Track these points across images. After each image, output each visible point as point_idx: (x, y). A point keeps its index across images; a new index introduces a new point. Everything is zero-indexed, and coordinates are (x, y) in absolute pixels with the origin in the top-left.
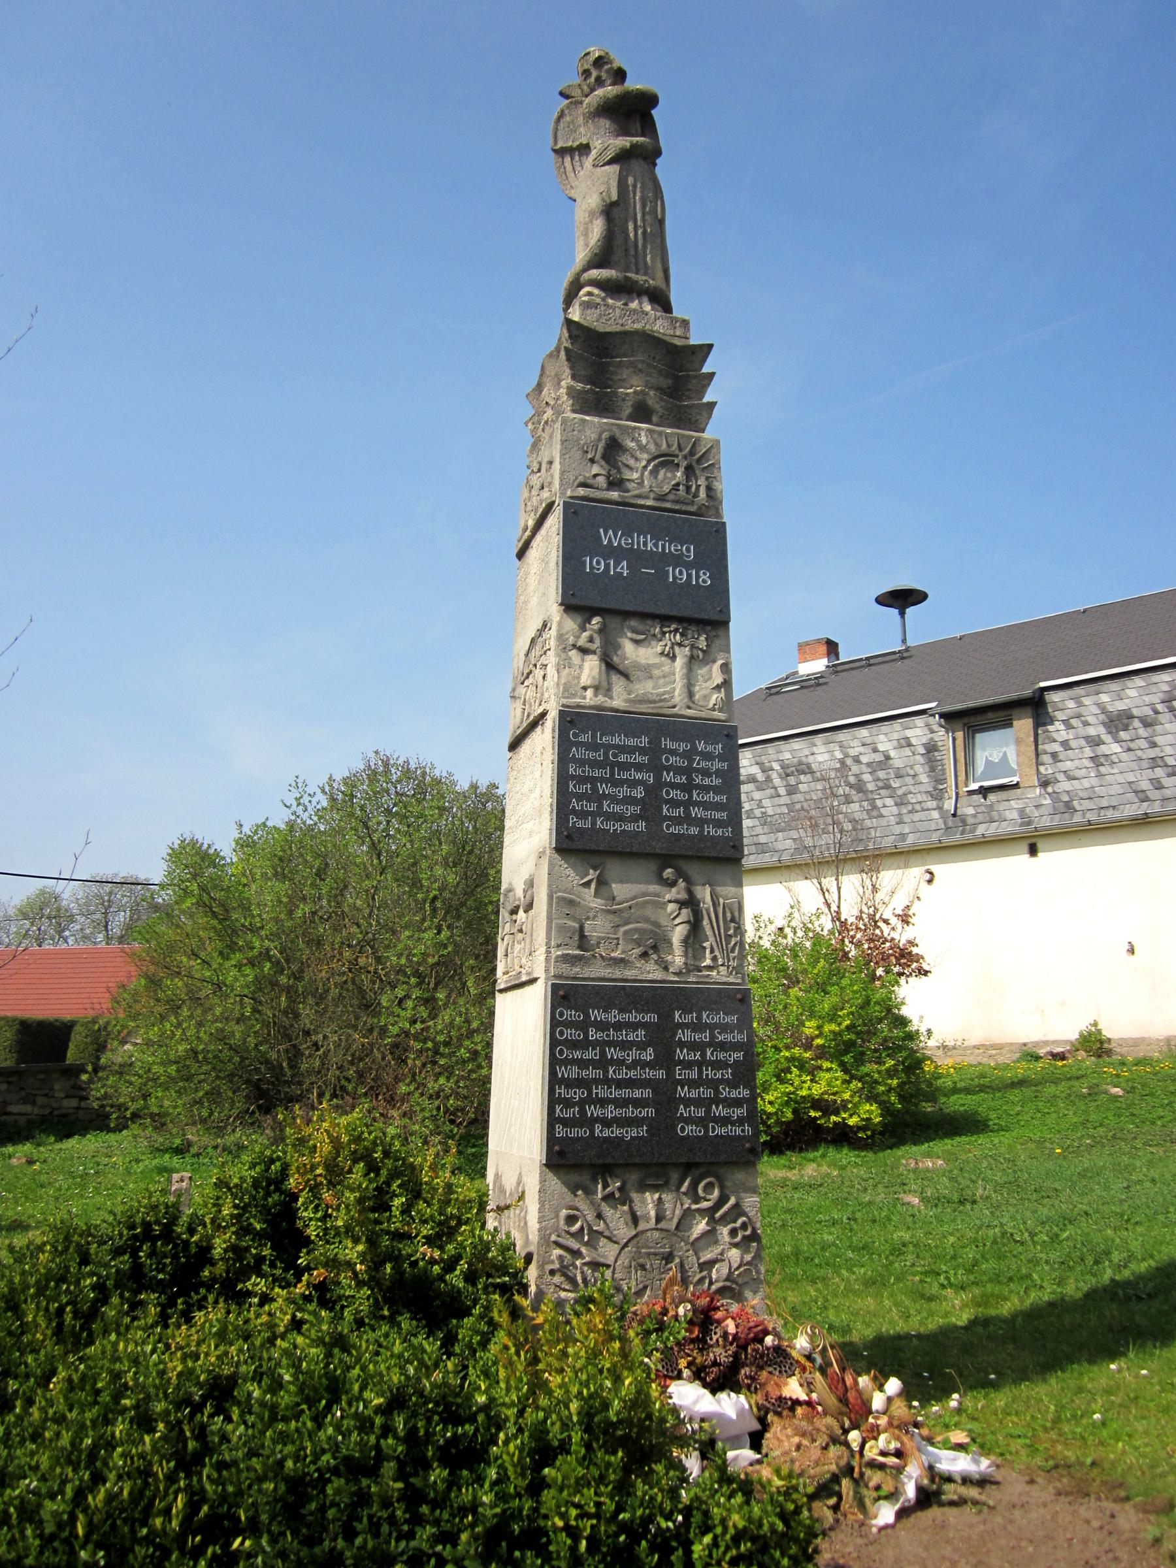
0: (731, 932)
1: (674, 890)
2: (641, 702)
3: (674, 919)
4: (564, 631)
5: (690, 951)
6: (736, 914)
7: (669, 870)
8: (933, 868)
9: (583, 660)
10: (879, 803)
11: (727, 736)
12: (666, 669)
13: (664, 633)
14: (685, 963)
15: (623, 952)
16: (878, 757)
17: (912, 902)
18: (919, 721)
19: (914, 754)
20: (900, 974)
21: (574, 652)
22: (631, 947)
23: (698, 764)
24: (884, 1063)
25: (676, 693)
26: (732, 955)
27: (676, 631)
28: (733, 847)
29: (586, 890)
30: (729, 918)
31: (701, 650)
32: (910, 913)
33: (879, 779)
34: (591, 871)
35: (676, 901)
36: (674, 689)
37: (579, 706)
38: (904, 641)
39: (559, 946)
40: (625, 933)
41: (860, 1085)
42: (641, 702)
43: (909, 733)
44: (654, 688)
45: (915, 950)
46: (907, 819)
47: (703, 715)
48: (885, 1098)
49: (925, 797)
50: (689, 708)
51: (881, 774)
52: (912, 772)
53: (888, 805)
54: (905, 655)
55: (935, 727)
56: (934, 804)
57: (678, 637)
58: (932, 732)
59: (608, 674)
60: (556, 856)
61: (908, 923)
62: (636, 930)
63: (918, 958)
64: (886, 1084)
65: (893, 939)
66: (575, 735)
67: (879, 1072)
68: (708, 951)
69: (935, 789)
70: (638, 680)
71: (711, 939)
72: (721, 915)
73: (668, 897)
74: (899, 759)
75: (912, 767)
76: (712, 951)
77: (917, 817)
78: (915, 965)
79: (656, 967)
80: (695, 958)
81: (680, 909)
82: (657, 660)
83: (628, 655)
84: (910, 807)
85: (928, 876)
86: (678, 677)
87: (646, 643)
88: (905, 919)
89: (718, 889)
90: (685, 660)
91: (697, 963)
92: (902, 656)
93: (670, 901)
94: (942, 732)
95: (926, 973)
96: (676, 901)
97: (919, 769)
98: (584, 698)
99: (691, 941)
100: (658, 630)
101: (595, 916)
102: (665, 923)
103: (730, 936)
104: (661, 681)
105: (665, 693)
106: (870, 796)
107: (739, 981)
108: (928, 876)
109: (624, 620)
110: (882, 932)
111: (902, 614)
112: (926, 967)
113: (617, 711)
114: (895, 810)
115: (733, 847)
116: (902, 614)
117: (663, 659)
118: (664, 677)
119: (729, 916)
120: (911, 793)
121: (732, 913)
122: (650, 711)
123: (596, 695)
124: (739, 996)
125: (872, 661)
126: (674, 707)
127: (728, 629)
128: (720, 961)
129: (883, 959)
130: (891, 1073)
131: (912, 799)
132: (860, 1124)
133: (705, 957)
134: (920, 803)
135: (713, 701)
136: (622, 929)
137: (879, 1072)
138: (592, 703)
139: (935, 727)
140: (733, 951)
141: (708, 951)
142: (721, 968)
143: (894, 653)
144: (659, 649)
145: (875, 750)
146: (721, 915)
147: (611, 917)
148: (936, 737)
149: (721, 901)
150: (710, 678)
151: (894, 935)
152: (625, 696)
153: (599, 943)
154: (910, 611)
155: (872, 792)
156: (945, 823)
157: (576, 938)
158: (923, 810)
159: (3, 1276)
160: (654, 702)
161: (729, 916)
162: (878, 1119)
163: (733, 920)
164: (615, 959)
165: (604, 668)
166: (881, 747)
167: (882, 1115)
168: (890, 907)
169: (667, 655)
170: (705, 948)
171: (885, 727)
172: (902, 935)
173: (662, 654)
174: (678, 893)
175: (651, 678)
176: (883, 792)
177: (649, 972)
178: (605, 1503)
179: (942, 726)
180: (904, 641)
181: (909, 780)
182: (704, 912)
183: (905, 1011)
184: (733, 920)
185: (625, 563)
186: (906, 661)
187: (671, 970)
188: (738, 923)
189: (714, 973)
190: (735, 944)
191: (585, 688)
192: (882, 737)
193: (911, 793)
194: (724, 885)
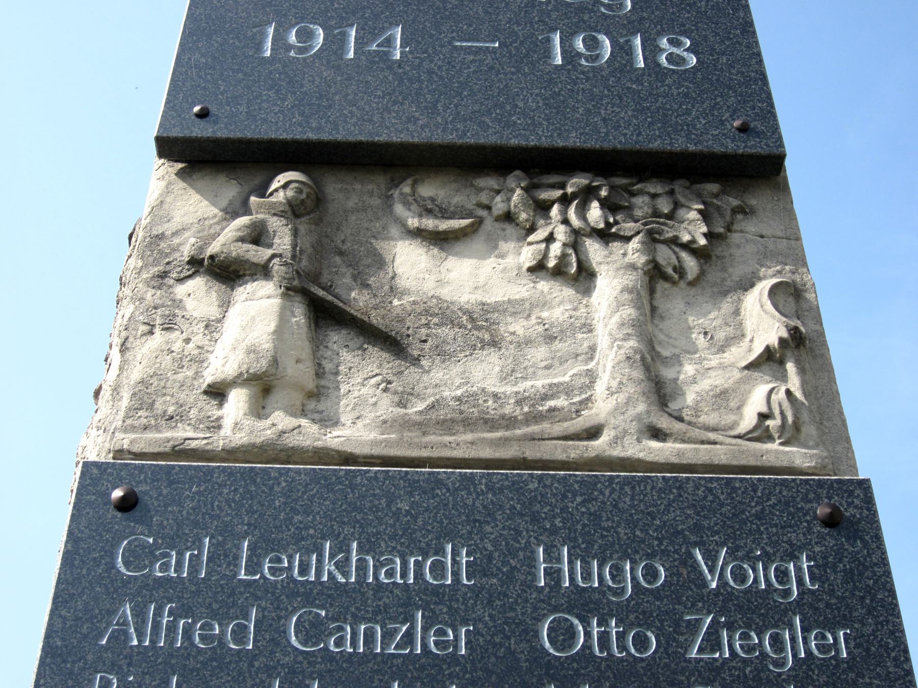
2: (447, 426)
4: (168, 228)
9: (225, 305)
11: (832, 521)
12: (557, 314)
13: (543, 208)
21: (198, 284)
23: (712, 642)
25: (600, 388)
27: (586, 195)
31: (689, 247)
36: (592, 376)
37: (179, 452)
42: (447, 426)
44: (504, 378)
47: (720, 454)
50: (657, 434)
57: (595, 213)
59: (317, 344)
66: (133, 559)
70: (443, 354)
82: (522, 290)
83: (402, 283)
86: (603, 336)
87: (478, 243)
90: (631, 279)
98: (216, 425)
100: (517, 196)
104: (539, 353)
105: (552, 392)
109: (395, 183)
113: (348, 459)
117: (544, 285)
118: (550, 338)
122: (487, 453)
123: (259, 409)
126: (593, 433)
127: (783, 188)
135: (755, 403)
138: (240, 439)
144: (527, 255)
150: (738, 336)
152: (386, 408)
160: (510, 422)
165: (299, 316)
169: (559, 272)
173: (538, 268)
175: (495, 343)
178: (715, 130)
185: (398, 32)
191: (218, 392)
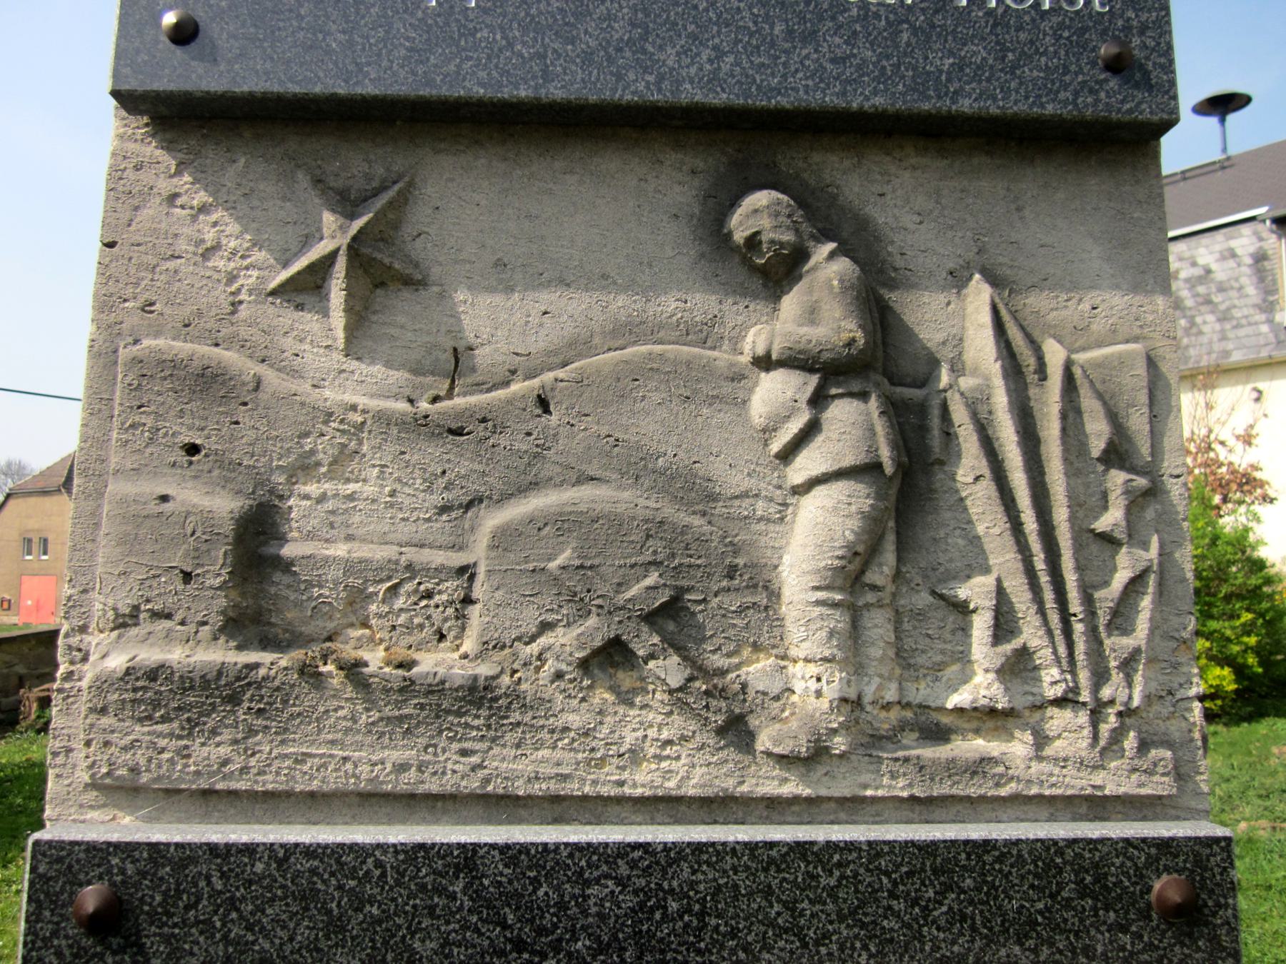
0: (1112, 519)
1: (791, 303)
3: (787, 454)
5: (878, 626)
6: (1138, 422)
7: (761, 198)
8: (1260, 385)
10: (1198, 320)
14: (850, 703)
15: (490, 647)
16: (1197, 272)
17: (1256, 421)
18: (1246, 229)
19: (1239, 265)
20: (1240, 502)
22: (530, 618)
24: (1239, 617)
26: (1118, 646)
28: (1116, 66)
29: (309, 321)
30: (1097, 446)
32: (1254, 432)
33: (1198, 295)
34: (329, 219)
35: (796, 361)
38: (1224, 150)
39: (124, 621)
40: (503, 540)
41: (1208, 644)
43: (1233, 244)
45: (1258, 475)
46: (1231, 335)
48: (1240, 660)
49: (1252, 311)
51: (1201, 289)
52: (1236, 285)
53: (1208, 322)
54: (1226, 164)
55: (1265, 234)
56: (1263, 317)
58: (1261, 239)
60: (152, 150)
61: (1250, 444)
62: (563, 523)
63: (1262, 484)
64: (1239, 643)
65: (1230, 464)
67: (1233, 628)
68: (981, 626)
69: (1264, 300)
71: (1003, 558)
72: (1051, 430)
73: (755, 340)
74: (1221, 272)
75: (1237, 280)
76: (1004, 626)
77: (1242, 332)
78: (1259, 491)
79: (679, 724)
80: (903, 657)
81: (819, 400)
84: (1234, 323)
85: (1255, 395)
88: (1247, 439)
89: (1036, 302)
91: (920, 692)
92: (1224, 165)
93: (765, 363)
94: (1273, 238)
95: (1272, 500)
96: (796, 361)
97: (1245, 281)
99: (880, 574)
101: (344, 457)
102: (736, 481)
103: (1108, 539)
106: (1188, 313)
107: (1160, 785)
108: (1255, 395)
110: (1217, 455)
111: (1222, 121)
112: (1272, 494)
114: (1218, 327)
115: (1116, 66)
116: (1222, 121)
119: (1097, 432)
120: (1235, 307)
121: (1113, 417)
124: (1165, 886)
125: (1188, 175)
128: (1051, 681)
129: (1220, 485)
130: (1248, 630)
131: (1237, 313)
132: (1208, 692)
133: (963, 658)
134: (1246, 317)
136: (493, 520)
137: (1233, 628)
139: (1265, 234)
140: (1121, 617)
141: (981, 626)
142: (1058, 719)
143: (1214, 163)
145: (1194, 264)
146: (1051, 430)
147: (432, 454)
148: (1266, 245)
149: (1055, 354)
151: (1235, 459)
153: (358, 598)
154: (1232, 118)
155: (1190, 309)
156: (1276, 336)
157: (216, 571)
158: (1250, 324)
159: (40, 959)
161: (1097, 432)
162: (1233, 687)
163: (1117, 455)
164: (437, 688)
166: (1201, 261)
167: (1236, 681)
168: (1229, 427)
170: (963, 609)
171: (1205, 239)
172: (1241, 458)
174: (811, 314)
176: (1203, 308)
177: (635, 756)
179: (1272, 231)
180: (1224, 150)
181: (1233, 294)
182: (959, 414)
183: (1262, 553)
184: (1117, 455)
186: (1227, 171)
187: (763, 742)
188: (1151, 471)
189: (1018, 748)
190: (1135, 584)
192: (1202, 250)
193: (1235, 307)
194: (1074, 286)
